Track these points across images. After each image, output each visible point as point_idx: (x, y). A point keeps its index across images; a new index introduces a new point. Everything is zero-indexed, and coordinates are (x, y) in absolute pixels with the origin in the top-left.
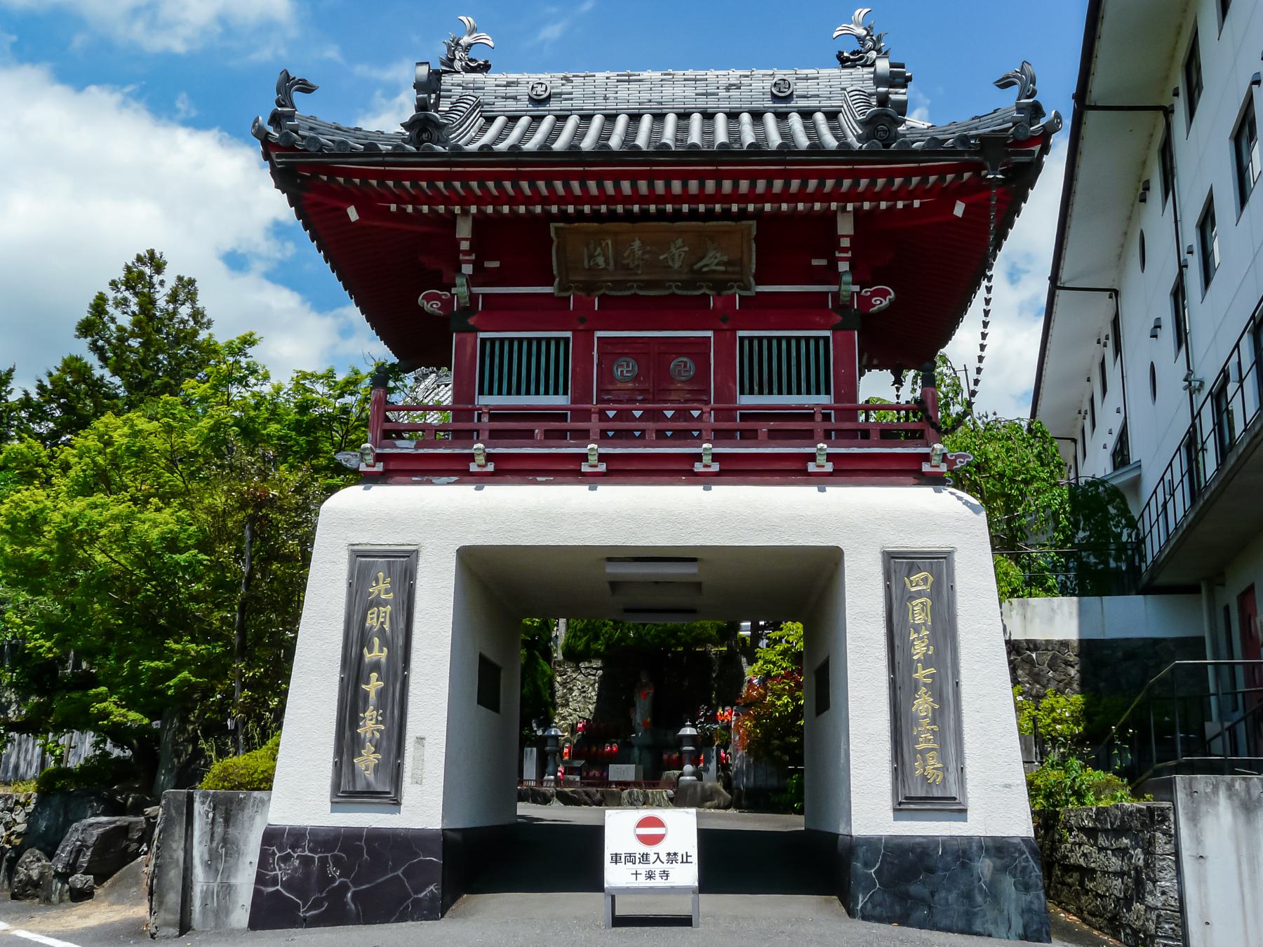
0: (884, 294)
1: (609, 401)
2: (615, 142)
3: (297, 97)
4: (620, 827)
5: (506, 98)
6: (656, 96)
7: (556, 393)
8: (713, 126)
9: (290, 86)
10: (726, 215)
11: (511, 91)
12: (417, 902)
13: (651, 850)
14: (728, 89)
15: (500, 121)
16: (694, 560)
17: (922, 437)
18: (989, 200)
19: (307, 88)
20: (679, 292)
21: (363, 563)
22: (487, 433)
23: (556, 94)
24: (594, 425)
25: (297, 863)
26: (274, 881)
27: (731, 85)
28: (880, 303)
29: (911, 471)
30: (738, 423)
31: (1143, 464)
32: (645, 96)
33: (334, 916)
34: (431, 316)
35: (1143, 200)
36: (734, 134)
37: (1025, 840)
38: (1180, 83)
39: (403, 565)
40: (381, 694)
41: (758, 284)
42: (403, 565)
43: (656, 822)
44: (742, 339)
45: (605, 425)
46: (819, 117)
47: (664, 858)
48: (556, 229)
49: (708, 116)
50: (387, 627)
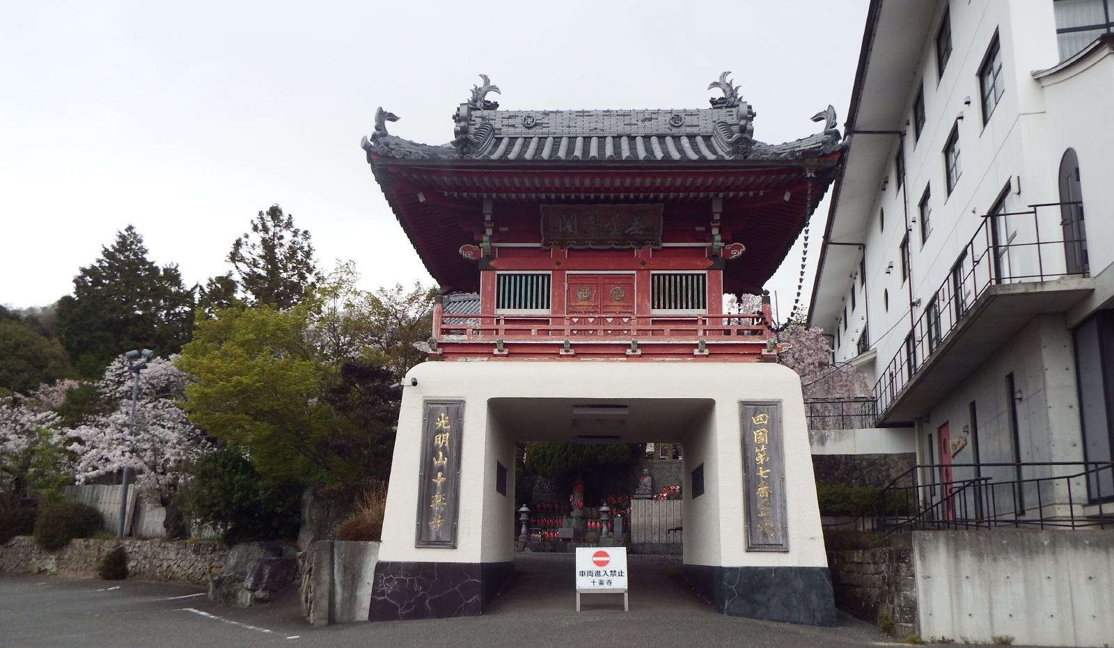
0: (739, 248)
1: (574, 312)
2: (545, 154)
3: (388, 124)
4: (584, 557)
5: (509, 126)
6: (600, 126)
7: (543, 307)
8: (635, 144)
9: (384, 117)
10: (646, 200)
11: (511, 122)
12: (467, 605)
13: (601, 569)
14: (644, 121)
15: (505, 141)
16: (626, 407)
17: (761, 334)
18: (806, 191)
19: (393, 118)
20: (616, 247)
21: (432, 408)
22: (503, 331)
23: (539, 123)
24: (566, 326)
25: (396, 583)
26: (383, 593)
27: (647, 119)
28: (736, 254)
29: (755, 353)
30: (650, 327)
31: (878, 350)
32: (593, 126)
33: (418, 613)
34: (468, 259)
35: (884, 189)
36: (649, 150)
37: (822, 569)
38: (911, 118)
39: (456, 409)
40: (444, 484)
41: (664, 242)
42: (456, 409)
43: (605, 555)
44: (653, 275)
45: (572, 327)
46: (699, 139)
47: (609, 573)
48: (543, 208)
49: (632, 139)
50: (447, 444)
